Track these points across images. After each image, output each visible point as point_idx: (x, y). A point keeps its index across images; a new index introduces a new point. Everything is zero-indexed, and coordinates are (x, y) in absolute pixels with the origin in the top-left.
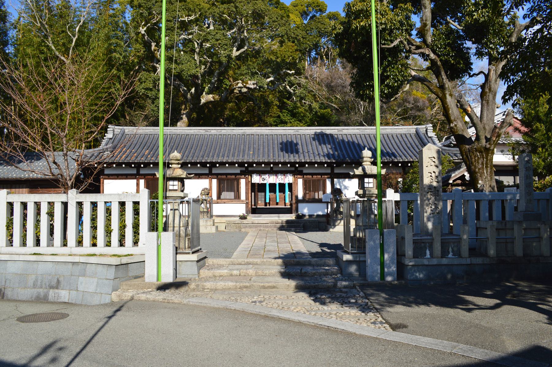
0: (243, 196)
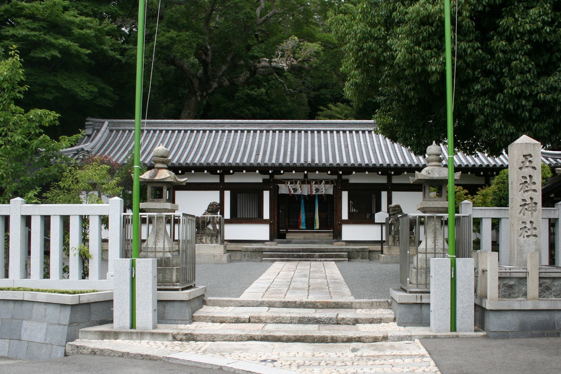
0: (266, 215)
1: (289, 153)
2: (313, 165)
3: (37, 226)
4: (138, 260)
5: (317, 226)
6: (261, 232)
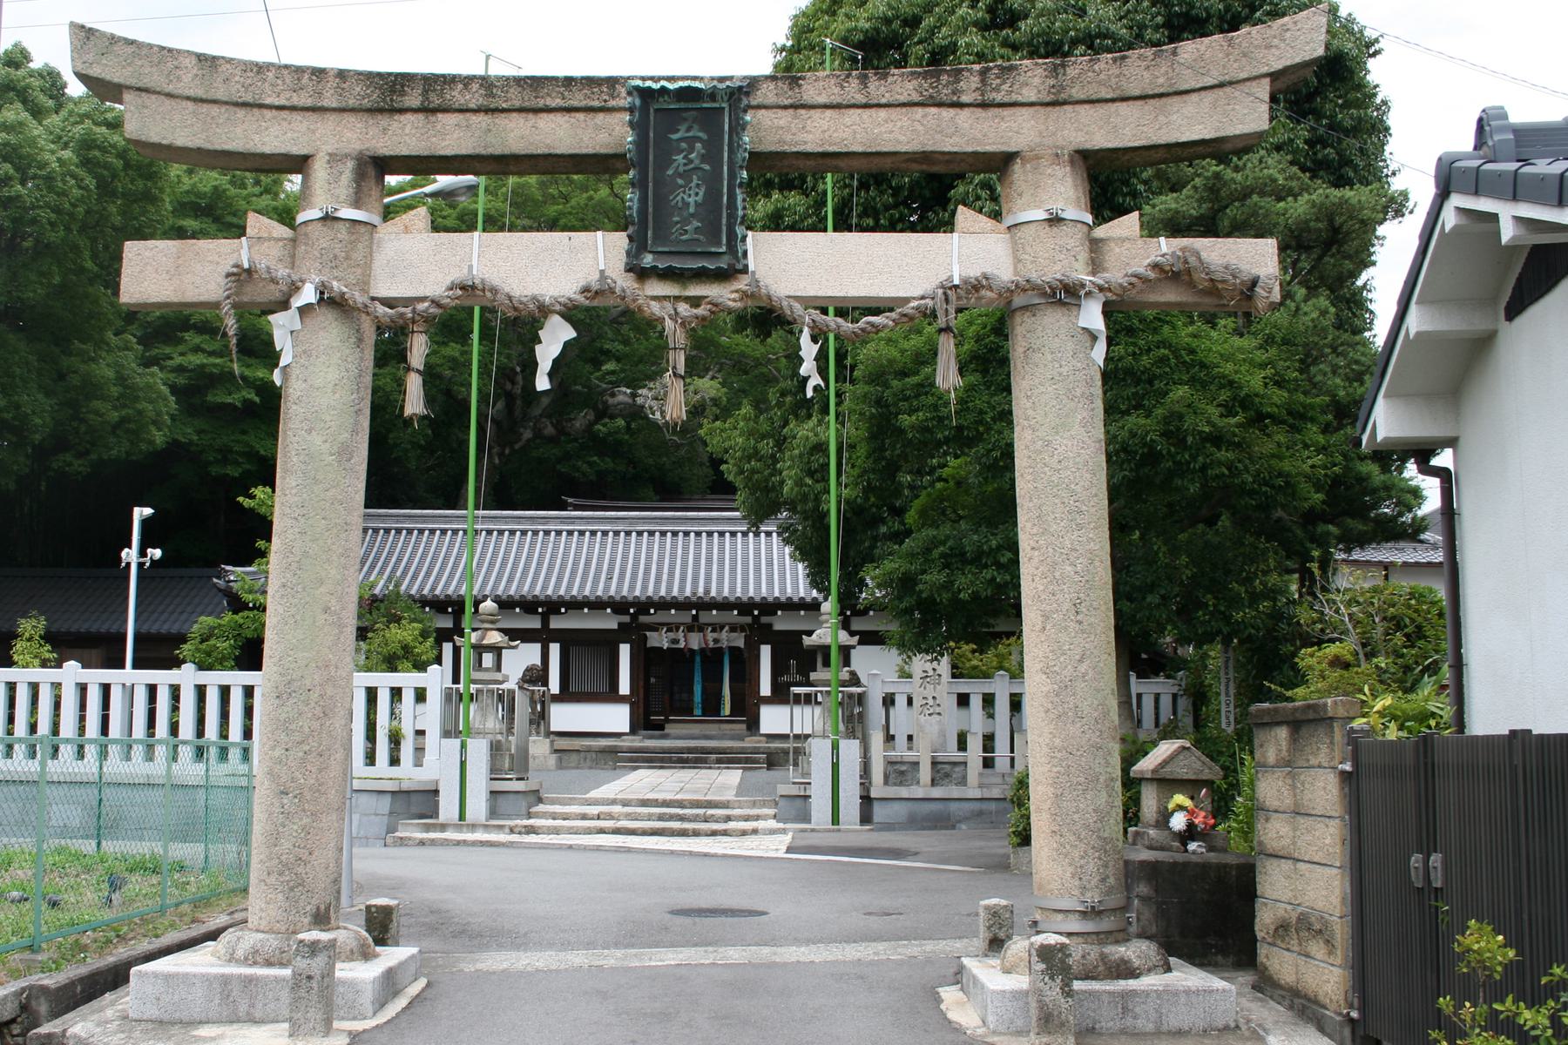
0: (624, 688)
1: (665, 577)
2: (707, 599)
3: (213, 699)
4: (469, 740)
5: (727, 710)
6: (614, 718)
